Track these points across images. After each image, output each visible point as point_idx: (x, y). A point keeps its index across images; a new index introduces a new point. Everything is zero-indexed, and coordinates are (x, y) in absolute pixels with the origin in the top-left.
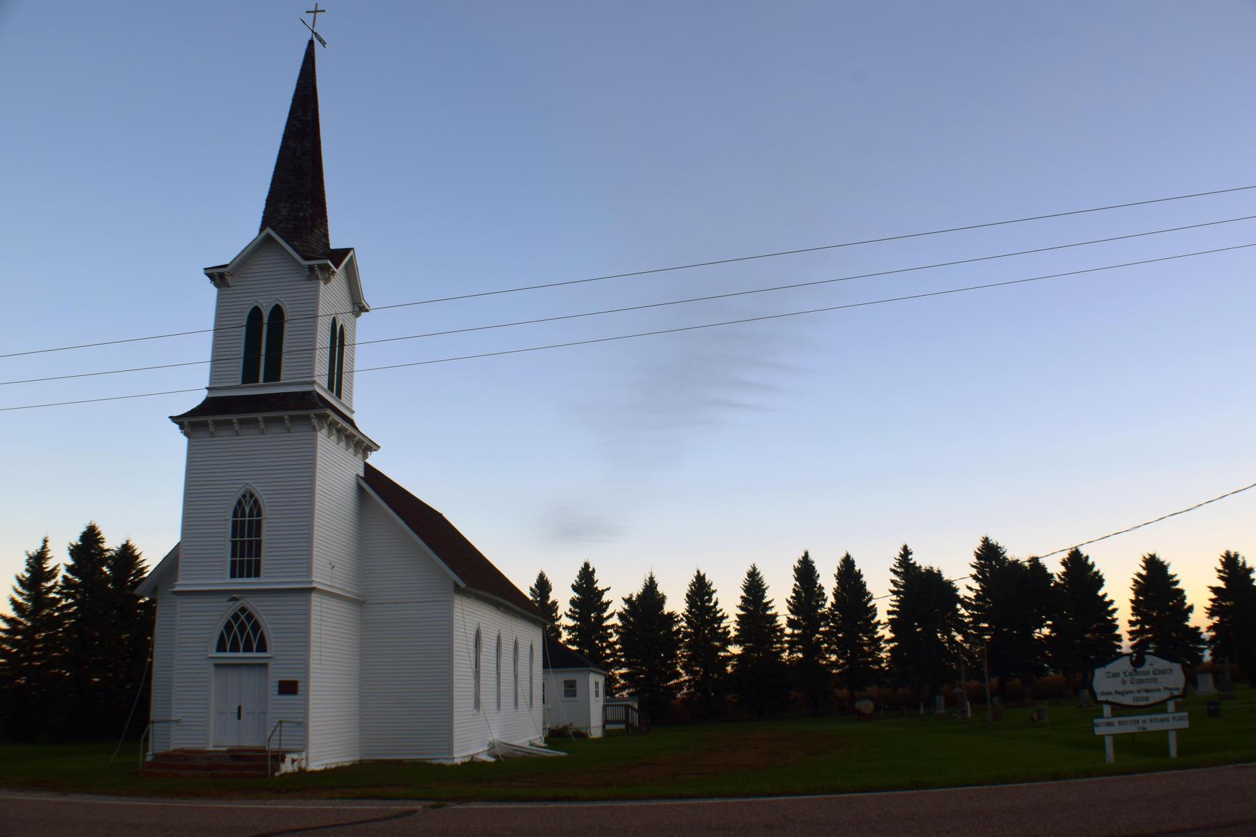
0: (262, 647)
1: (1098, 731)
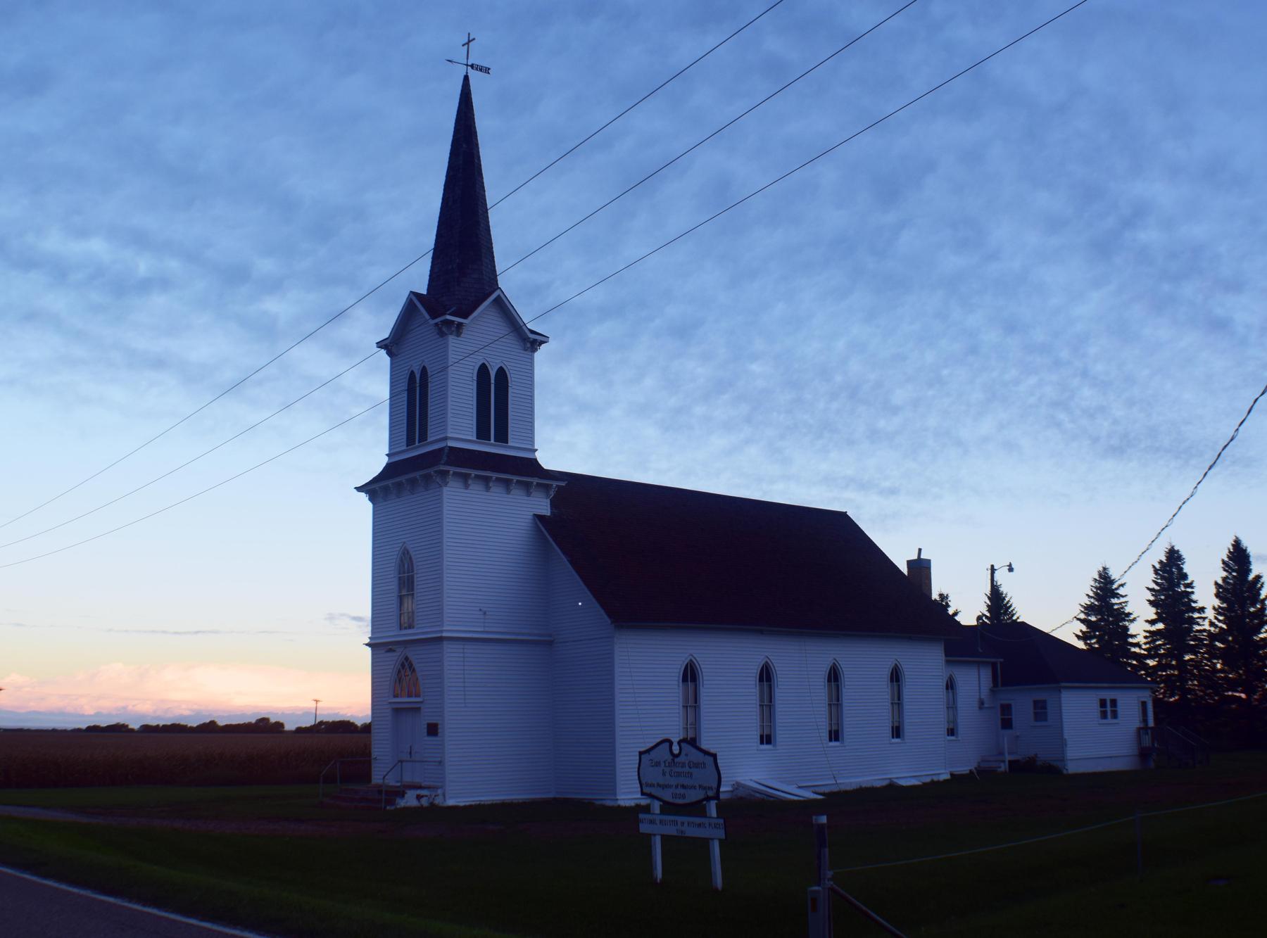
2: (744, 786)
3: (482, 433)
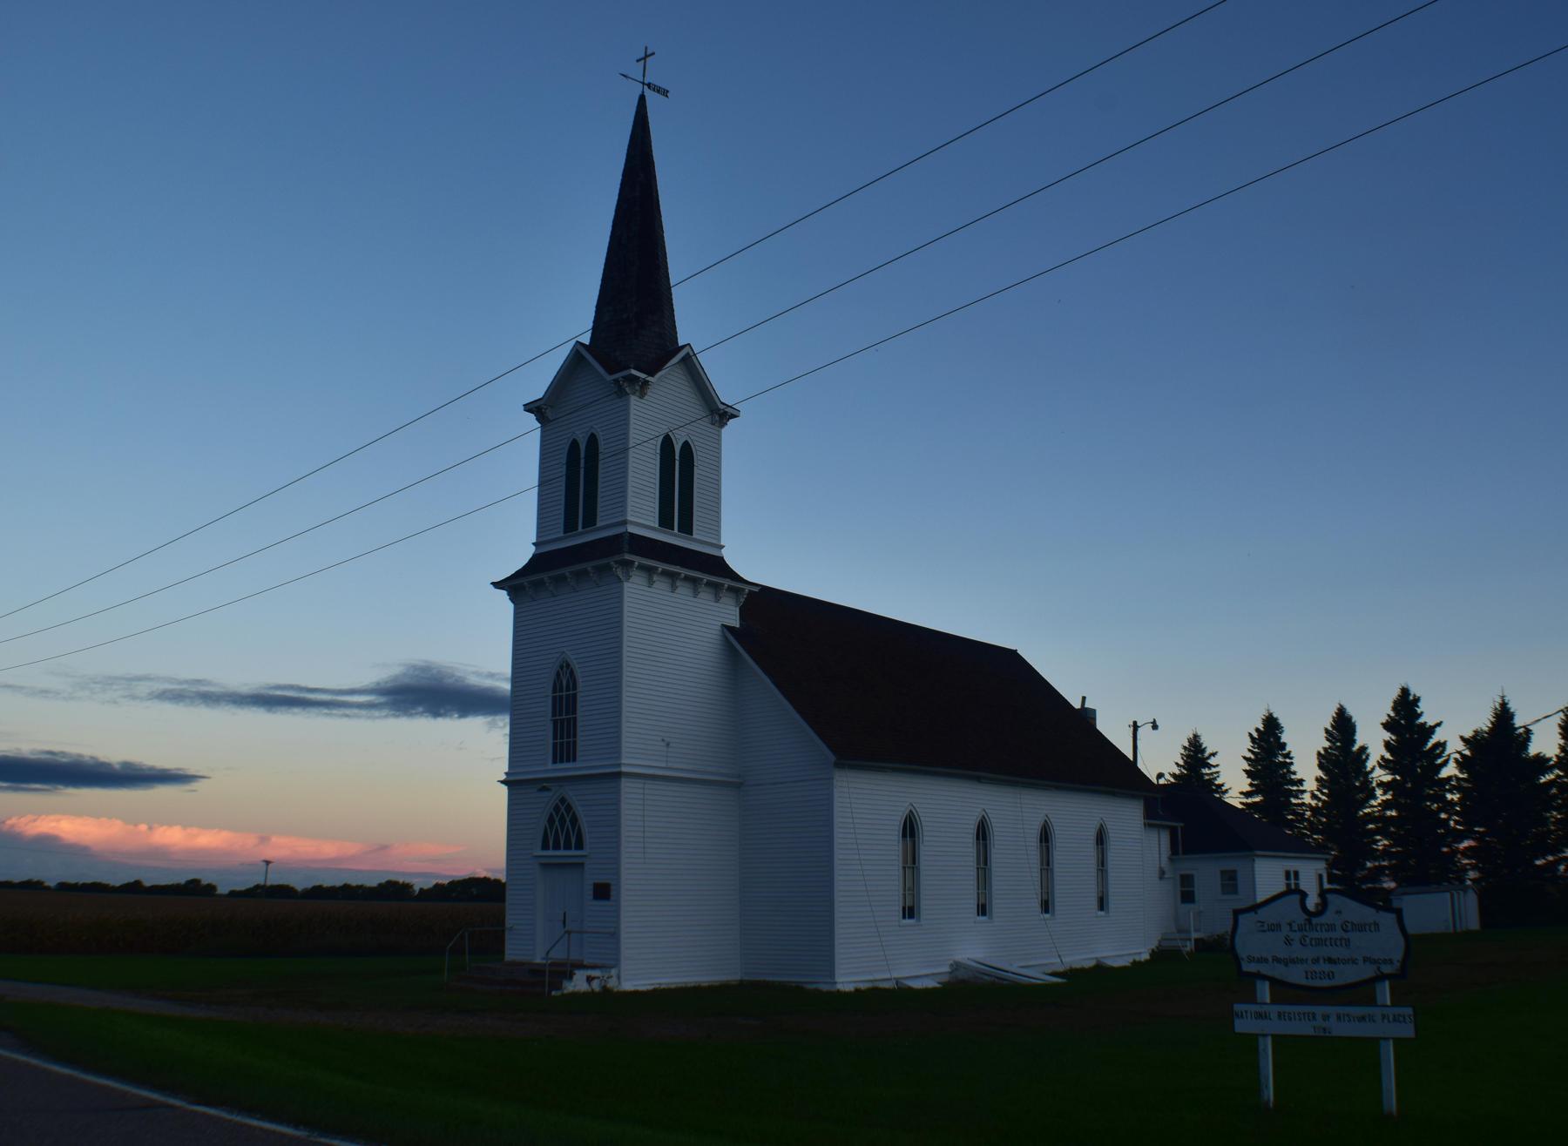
0: (579, 846)
1: (1241, 1026)
2: (966, 967)
3: (665, 521)
